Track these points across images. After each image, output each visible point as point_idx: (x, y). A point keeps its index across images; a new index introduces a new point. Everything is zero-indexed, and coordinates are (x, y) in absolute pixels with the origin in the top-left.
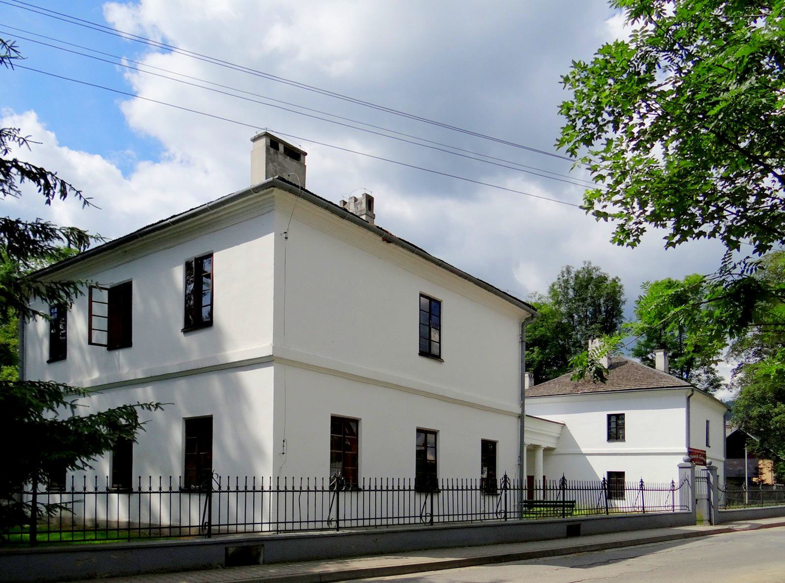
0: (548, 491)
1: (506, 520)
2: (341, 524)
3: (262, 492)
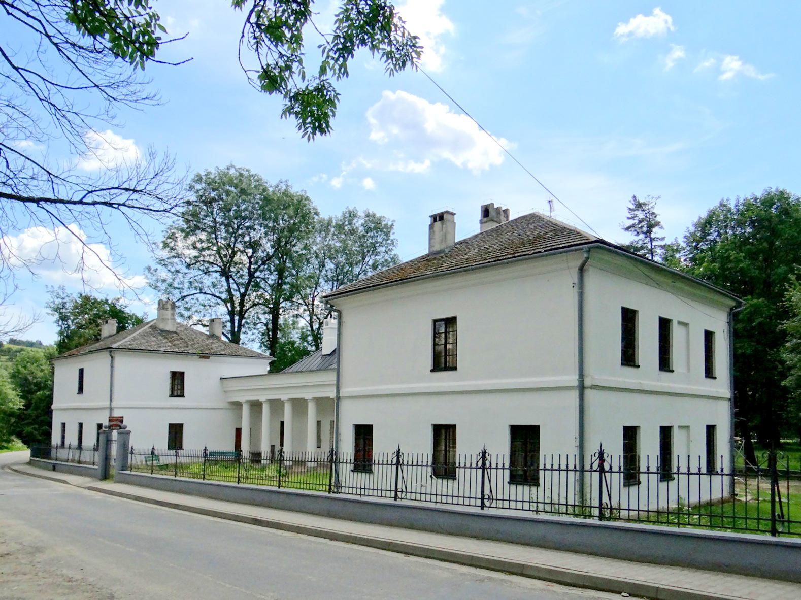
0: (341, 465)
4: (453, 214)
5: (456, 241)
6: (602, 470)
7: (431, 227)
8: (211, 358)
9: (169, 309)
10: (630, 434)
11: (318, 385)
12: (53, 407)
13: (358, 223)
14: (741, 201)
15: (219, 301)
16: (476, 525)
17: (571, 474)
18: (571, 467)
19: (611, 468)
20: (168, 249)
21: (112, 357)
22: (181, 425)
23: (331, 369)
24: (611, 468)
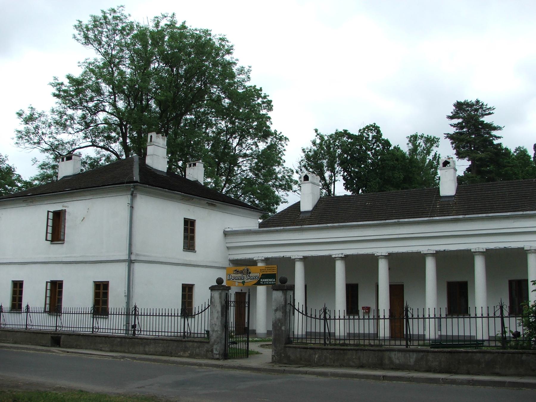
1: (407, 347)
3: (476, 318)
6: (135, 315)
11: (458, 235)
19: (330, 317)
24: (330, 317)
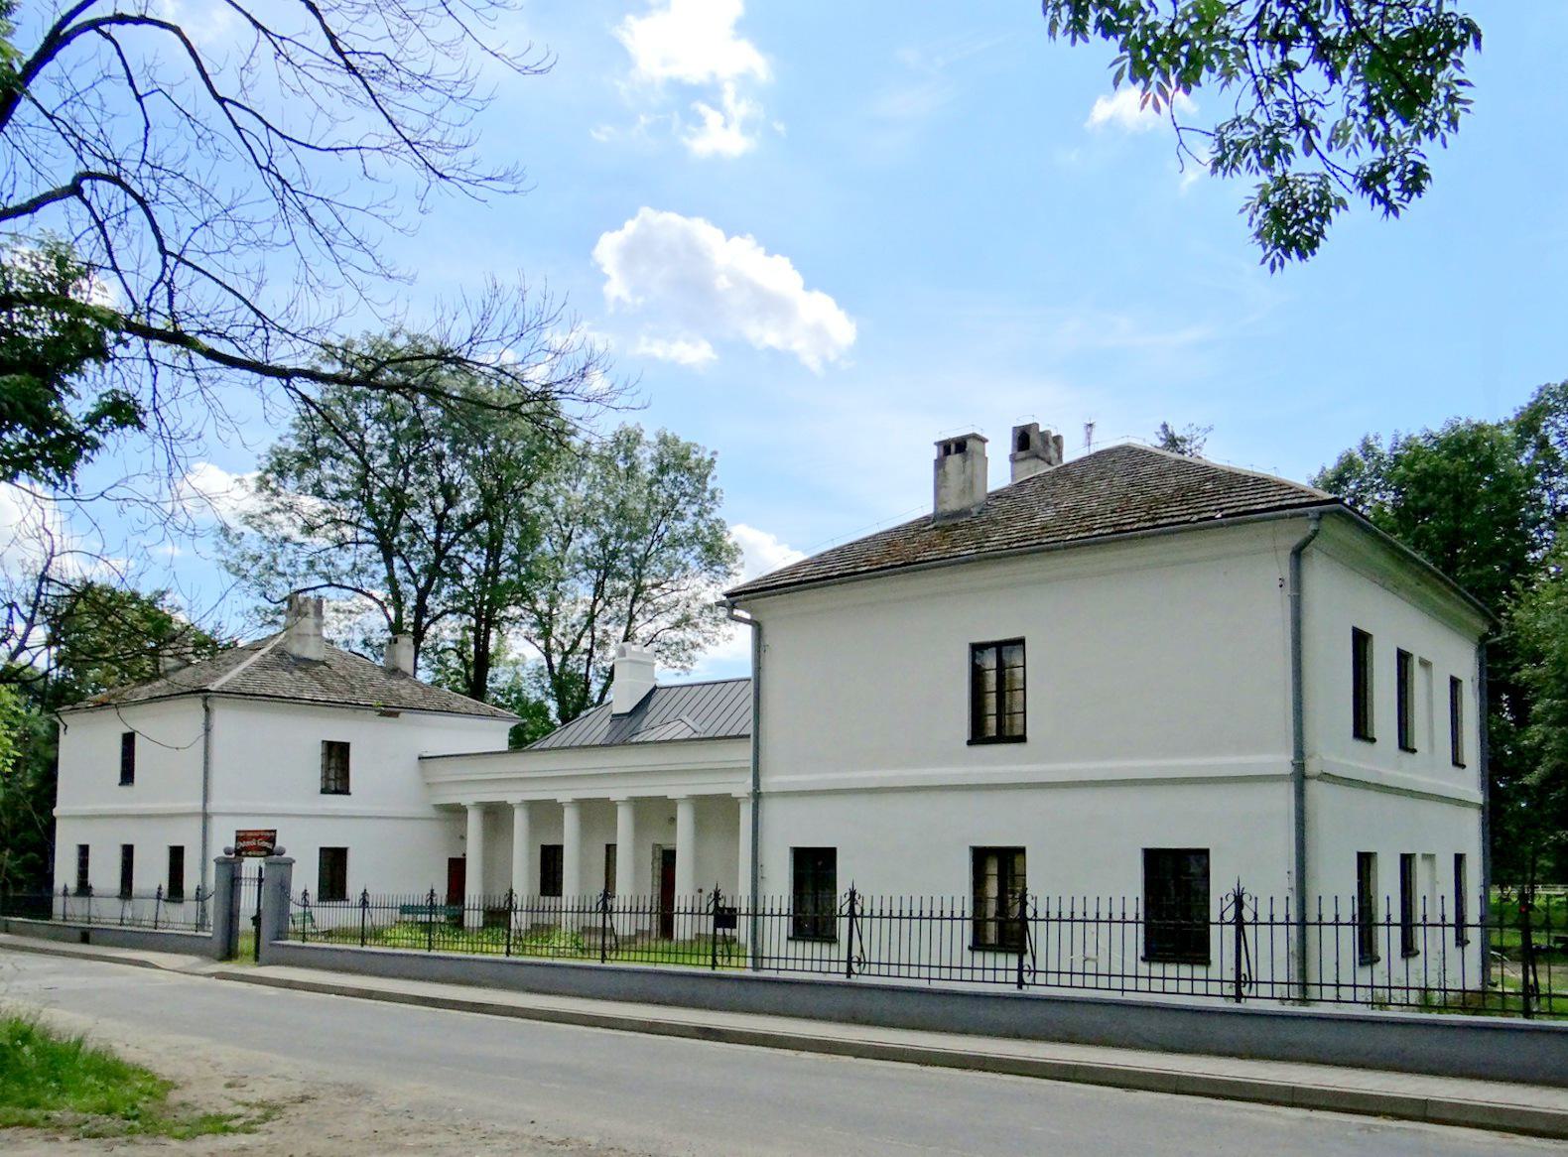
2: (1314, 992)
3: (1320, 925)
4: (984, 441)
5: (990, 490)
7: (940, 464)
8: (401, 715)
9: (312, 616)
10: (1365, 861)
12: (56, 812)
13: (645, 459)
14: (1402, 439)
15: (369, 602)
16: (1225, 1031)
17: (1280, 930)
18: (1280, 917)
20: (267, 493)
21: (207, 710)
22: (182, 848)
23: (632, 744)
